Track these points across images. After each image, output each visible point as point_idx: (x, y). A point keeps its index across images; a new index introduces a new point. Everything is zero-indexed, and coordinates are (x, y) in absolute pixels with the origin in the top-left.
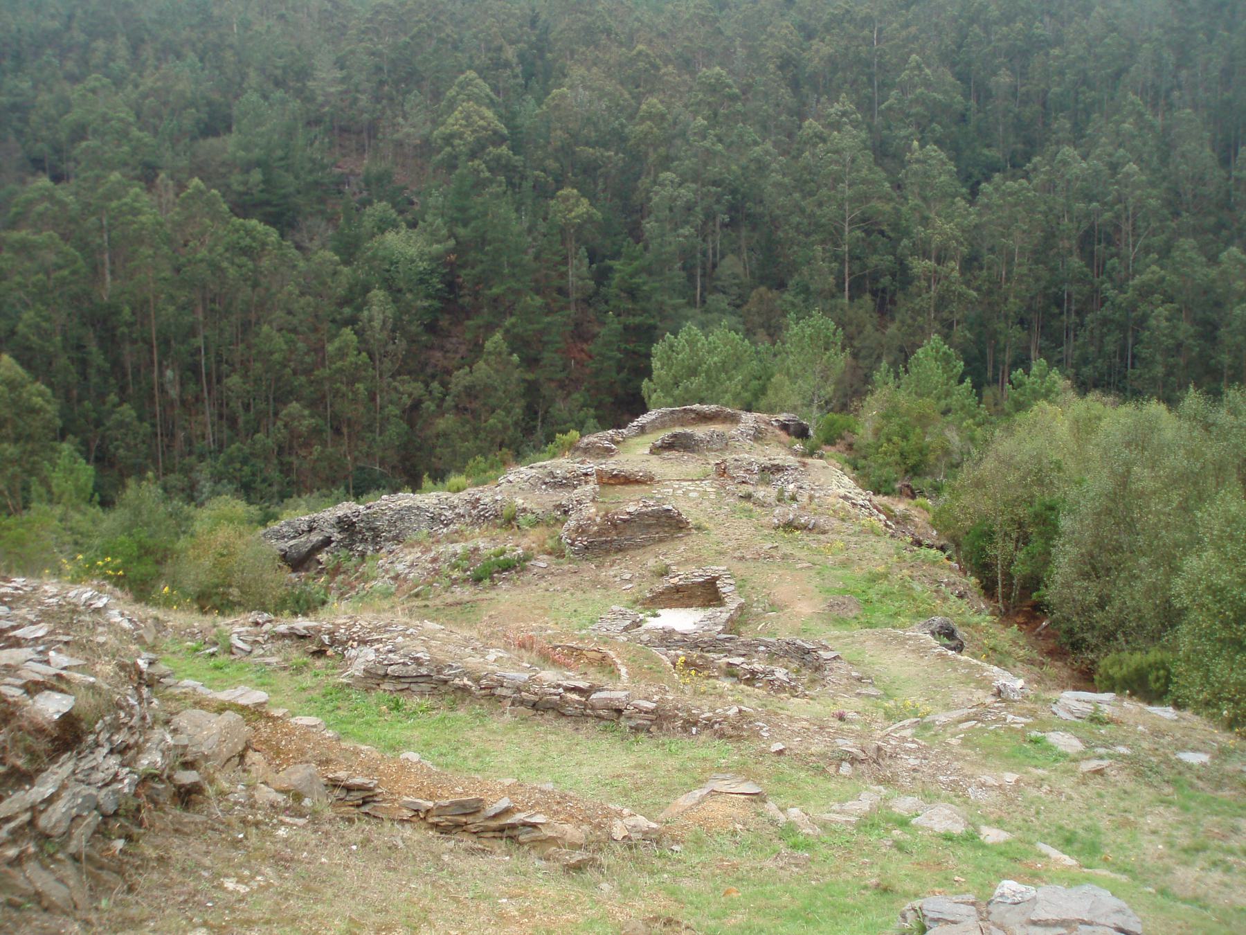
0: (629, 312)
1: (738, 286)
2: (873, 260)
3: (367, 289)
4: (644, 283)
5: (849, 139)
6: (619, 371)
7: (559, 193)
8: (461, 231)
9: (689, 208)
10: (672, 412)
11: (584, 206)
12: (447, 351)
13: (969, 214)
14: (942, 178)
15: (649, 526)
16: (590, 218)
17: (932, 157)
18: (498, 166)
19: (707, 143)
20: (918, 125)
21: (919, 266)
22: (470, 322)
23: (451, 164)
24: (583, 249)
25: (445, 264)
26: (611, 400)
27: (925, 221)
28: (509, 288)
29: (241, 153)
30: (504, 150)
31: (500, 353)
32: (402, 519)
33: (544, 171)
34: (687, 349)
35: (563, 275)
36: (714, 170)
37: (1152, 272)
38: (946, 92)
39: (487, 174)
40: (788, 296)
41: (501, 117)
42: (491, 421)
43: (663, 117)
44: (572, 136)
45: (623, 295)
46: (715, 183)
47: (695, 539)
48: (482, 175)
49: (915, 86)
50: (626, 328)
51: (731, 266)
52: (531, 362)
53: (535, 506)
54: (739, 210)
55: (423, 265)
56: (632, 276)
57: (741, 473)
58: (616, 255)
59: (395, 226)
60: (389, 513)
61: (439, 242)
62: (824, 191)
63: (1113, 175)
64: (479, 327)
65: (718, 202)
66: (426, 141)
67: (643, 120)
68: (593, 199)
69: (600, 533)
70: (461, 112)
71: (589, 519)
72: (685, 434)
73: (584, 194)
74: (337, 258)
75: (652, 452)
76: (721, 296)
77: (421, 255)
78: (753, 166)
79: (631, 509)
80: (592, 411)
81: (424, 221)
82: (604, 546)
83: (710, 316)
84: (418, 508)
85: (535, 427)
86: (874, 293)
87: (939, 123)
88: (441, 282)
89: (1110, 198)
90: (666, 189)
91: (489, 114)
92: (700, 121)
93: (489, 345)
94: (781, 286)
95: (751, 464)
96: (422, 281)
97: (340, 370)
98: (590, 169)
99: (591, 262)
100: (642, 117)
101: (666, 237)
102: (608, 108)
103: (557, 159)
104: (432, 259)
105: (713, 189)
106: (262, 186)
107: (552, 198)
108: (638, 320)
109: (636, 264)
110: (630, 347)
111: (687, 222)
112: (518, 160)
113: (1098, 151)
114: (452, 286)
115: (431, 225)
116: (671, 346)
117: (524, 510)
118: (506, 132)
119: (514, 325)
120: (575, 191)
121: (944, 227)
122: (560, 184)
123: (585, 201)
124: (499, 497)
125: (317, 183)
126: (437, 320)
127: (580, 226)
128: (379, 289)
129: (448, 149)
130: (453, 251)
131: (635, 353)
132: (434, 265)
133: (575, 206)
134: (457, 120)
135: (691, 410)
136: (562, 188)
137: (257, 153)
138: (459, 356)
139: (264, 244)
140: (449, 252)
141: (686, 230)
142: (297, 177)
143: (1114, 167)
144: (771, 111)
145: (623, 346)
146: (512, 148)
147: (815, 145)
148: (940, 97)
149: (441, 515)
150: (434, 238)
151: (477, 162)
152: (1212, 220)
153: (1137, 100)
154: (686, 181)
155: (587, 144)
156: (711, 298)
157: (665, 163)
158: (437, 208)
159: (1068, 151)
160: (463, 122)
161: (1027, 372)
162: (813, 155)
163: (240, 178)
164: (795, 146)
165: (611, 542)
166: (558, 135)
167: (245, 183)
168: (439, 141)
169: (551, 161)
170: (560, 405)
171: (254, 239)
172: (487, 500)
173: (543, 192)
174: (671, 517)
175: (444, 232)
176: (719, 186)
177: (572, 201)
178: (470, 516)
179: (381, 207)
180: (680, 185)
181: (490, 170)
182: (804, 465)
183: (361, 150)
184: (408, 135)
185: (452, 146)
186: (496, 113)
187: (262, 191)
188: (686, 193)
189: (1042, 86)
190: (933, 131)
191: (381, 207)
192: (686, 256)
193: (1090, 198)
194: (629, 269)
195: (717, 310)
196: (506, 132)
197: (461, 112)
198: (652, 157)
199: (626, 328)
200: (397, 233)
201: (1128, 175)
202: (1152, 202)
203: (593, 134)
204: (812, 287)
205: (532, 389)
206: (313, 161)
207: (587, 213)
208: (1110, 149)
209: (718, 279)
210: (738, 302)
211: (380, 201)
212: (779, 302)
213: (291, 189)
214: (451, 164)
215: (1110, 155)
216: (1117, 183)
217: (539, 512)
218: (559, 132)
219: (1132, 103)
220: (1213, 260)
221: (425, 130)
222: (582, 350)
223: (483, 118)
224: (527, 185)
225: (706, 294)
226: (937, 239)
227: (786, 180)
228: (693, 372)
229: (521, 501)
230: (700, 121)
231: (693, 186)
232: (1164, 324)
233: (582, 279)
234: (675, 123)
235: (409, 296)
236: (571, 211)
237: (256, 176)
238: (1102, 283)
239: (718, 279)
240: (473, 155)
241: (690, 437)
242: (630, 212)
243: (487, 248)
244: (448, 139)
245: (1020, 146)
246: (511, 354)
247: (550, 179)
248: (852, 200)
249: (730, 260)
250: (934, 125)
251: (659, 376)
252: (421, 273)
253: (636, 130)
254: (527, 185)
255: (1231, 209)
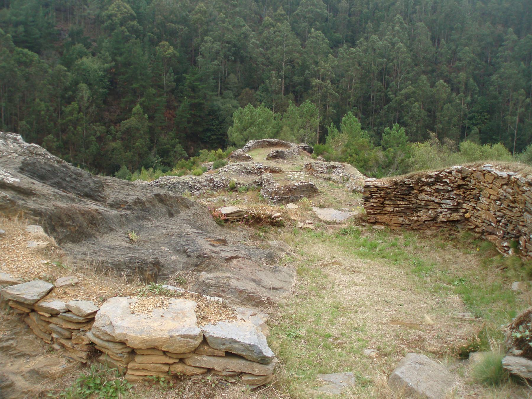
0: (193, 97)
1: (237, 87)
2: (296, 78)
3: (77, 83)
4: (199, 85)
5: (285, 26)
6: (189, 122)
7: (160, 44)
8: (119, 58)
9: (218, 52)
10: (259, 142)
11: (171, 50)
12: (111, 112)
13: (334, 61)
14: (324, 45)
15: (304, 191)
16: (174, 55)
17: (319, 36)
18: (133, 30)
19: (225, 25)
20: (309, 22)
21: (315, 82)
22: (124, 100)
23: (112, 28)
24: (171, 69)
25: (111, 73)
27: (316, 63)
28: (141, 85)
29: (14, 18)
30: (135, 23)
31: (140, 114)
32: (175, 187)
33: (152, 33)
36: (228, 36)
37: (410, 89)
38: (320, 9)
39: (128, 33)
40: (258, 93)
41: (133, 8)
43: (205, 12)
44: (165, 19)
46: (227, 42)
47: (322, 196)
48: (125, 34)
49: (308, 6)
51: (233, 78)
52: (151, 118)
53: (244, 182)
54: (237, 54)
55: (101, 73)
56: (194, 82)
57: (320, 169)
58: (186, 72)
59: (86, 55)
60: (168, 185)
61: (107, 63)
62: (274, 48)
63: (393, 48)
64: (127, 102)
65: (229, 51)
66: (98, 16)
67: (197, 13)
68: (175, 47)
69: (284, 194)
70: (115, 5)
71: (278, 188)
72: (281, 152)
73: (171, 44)
74: (66, 69)
75: (267, 159)
76: (231, 91)
77: (99, 68)
78: (242, 36)
79: (296, 184)
81: (100, 53)
82: (286, 200)
83: (225, 100)
84: (183, 182)
86: (294, 92)
87: (318, 21)
88: (108, 81)
89: (391, 57)
90: (209, 44)
91: (128, 6)
92: (222, 15)
93: (134, 110)
94: (256, 88)
95: (322, 165)
96: (100, 80)
97: (70, 121)
98: (173, 34)
100: (196, 12)
101: (207, 65)
102: (181, 7)
103: (158, 29)
104: (105, 71)
105: (227, 45)
106: (23, 34)
107: (156, 46)
108: (196, 101)
109: (196, 76)
110: (193, 112)
111: (216, 59)
112: (141, 28)
113: (386, 37)
114: (113, 82)
115: (104, 55)
117: (239, 184)
118: (135, 15)
119: (144, 101)
120: (167, 43)
121: (326, 66)
122: (160, 39)
123: (171, 47)
124: (223, 178)
125: (50, 34)
126: (106, 98)
127: (170, 58)
128: (83, 83)
129: (110, 21)
130: (114, 67)
131: (194, 115)
132: (106, 73)
133: (167, 49)
134: (114, 8)
135: (267, 141)
136: (161, 42)
137: (22, 18)
138: (116, 115)
139: (32, 61)
140: (111, 68)
141: (216, 62)
142: (40, 30)
143: (393, 44)
144: (248, 12)
146: (138, 22)
147: (269, 28)
148: (318, 10)
149: (194, 186)
150: (105, 61)
151: (123, 28)
152: (430, 68)
153: (401, 17)
154: (215, 41)
155: (172, 22)
156: (225, 92)
157: (206, 33)
158: (107, 48)
159: (375, 37)
160: (117, 9)
161: (391, 128)
162: (269, 32)
163: (13, 29)
164: (261, 28)
165: (289, 197)
166: (159, 18)
167: (16, 32)
168: (105, 17)
169: (156, 29)
170: (162, 137)
171: (27, 58)
172: (217, 179)
173: (153, 43)
174: (312, 187)
175: (110, 58)
176: (229, 44)
177: (166, 47)
178: (209, 186)
179: (79, 46)
180: (213, 42)
181: (129, 31)
182: (344, 166)
183: (66, 20)
184: (89, 14)
185: (112, 20)
186: (130, 6)
187: (24, 36)
188: (217, 46)
189: (360, 8)
190: (316, 25)
191: (79, 46)
192: (215, 73)
193: (383, 57)
194: (193, 78)
195: (228, 97)
196: (135, 15)
197: (115, 5)
198: (200, 30)
200: (88, 58)
201: (399, 48)
202: (409, 60)
203: (175, 18)
204: (270, 89)
205: (151, 131)
206: (49, 24)
207: (173, 52)
208: (391, 37)
209: (228, 84)
210: (237, 94)
211: (78, 43)
212: (255, 95)
213: (38, 36)
214: (112, 28)
215: (391, 39)
216: (395, 51)
217: (247, 184)
218: (160, 16)
219: (399, 18)
220: (433, 85)
221: (97, 12)
222: (170, 113)
223: (126, 8)
224: (146, 39)
225: (222, 90)
226: (322, 71)
227: (258, 42)
228: (252, 124)
229: (236, 180)
230: (222, 15)
231: (218, 43)
232: (417, 110)
233: (170, 82)
234: (211, 16)
235: (96, 87)
236: (165, 52)
237: (21, 29)
238: (388, 92)
239: (228, 84)
240: (121, 25)
241: (282, 153)
242: (191, 54)
243: (131, 67)
244: (110, 17)
245: (350, 33)
246: (144, 115)
247: (155, 37)
248: (287, 53)
249: (232, 76)
250: (316, 22)
252: (100, 77)
253: (193, 17)
254: (146, 39)
255: (436, 64)
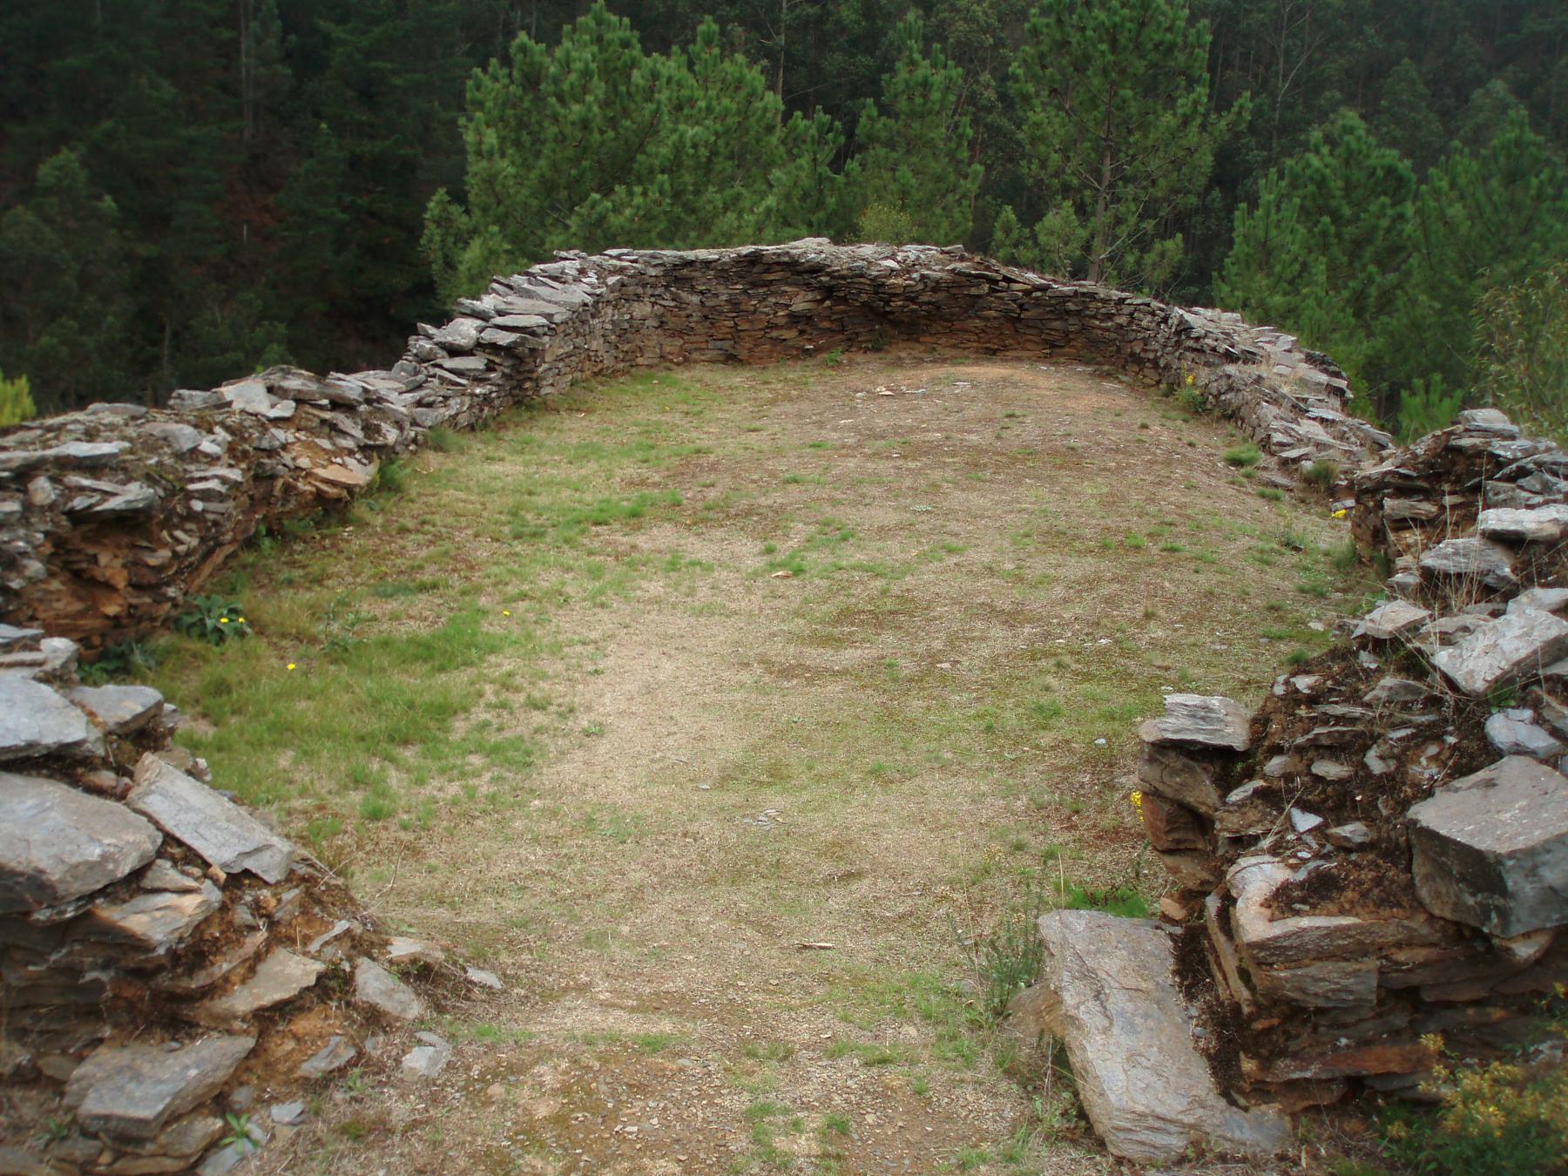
26: (322, 307)
34: (599, 88)
35: (230, 51)
42: (45, 340)
45: (350, 94)
50: (355, 162)
80: (281, 328)
85: (157, 359)
99: (286, 31)
108: (379, 146)
110: (363, 201)
116: (532, 80)
145: (348, 199)
199: (355, 162)
251: (490, 180)
